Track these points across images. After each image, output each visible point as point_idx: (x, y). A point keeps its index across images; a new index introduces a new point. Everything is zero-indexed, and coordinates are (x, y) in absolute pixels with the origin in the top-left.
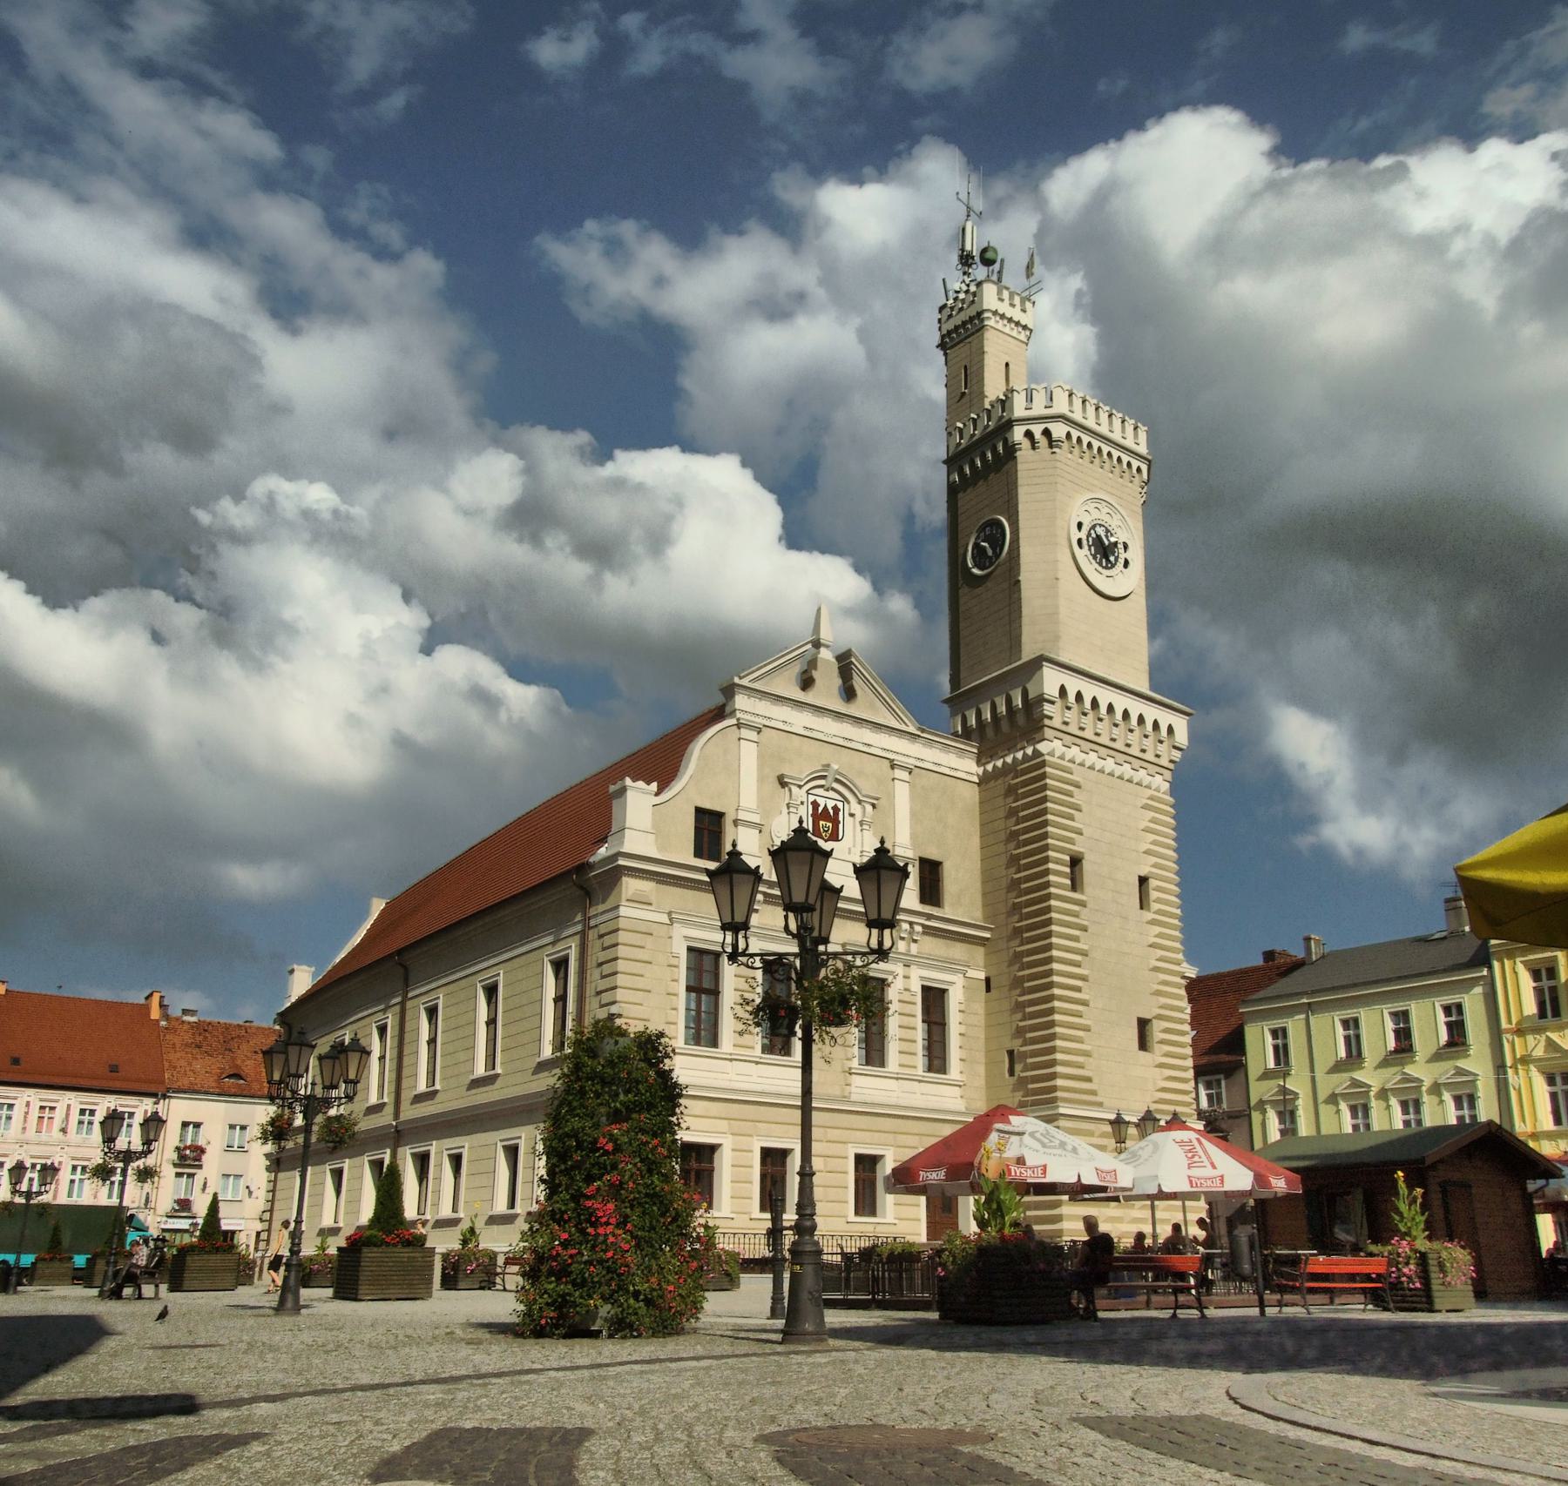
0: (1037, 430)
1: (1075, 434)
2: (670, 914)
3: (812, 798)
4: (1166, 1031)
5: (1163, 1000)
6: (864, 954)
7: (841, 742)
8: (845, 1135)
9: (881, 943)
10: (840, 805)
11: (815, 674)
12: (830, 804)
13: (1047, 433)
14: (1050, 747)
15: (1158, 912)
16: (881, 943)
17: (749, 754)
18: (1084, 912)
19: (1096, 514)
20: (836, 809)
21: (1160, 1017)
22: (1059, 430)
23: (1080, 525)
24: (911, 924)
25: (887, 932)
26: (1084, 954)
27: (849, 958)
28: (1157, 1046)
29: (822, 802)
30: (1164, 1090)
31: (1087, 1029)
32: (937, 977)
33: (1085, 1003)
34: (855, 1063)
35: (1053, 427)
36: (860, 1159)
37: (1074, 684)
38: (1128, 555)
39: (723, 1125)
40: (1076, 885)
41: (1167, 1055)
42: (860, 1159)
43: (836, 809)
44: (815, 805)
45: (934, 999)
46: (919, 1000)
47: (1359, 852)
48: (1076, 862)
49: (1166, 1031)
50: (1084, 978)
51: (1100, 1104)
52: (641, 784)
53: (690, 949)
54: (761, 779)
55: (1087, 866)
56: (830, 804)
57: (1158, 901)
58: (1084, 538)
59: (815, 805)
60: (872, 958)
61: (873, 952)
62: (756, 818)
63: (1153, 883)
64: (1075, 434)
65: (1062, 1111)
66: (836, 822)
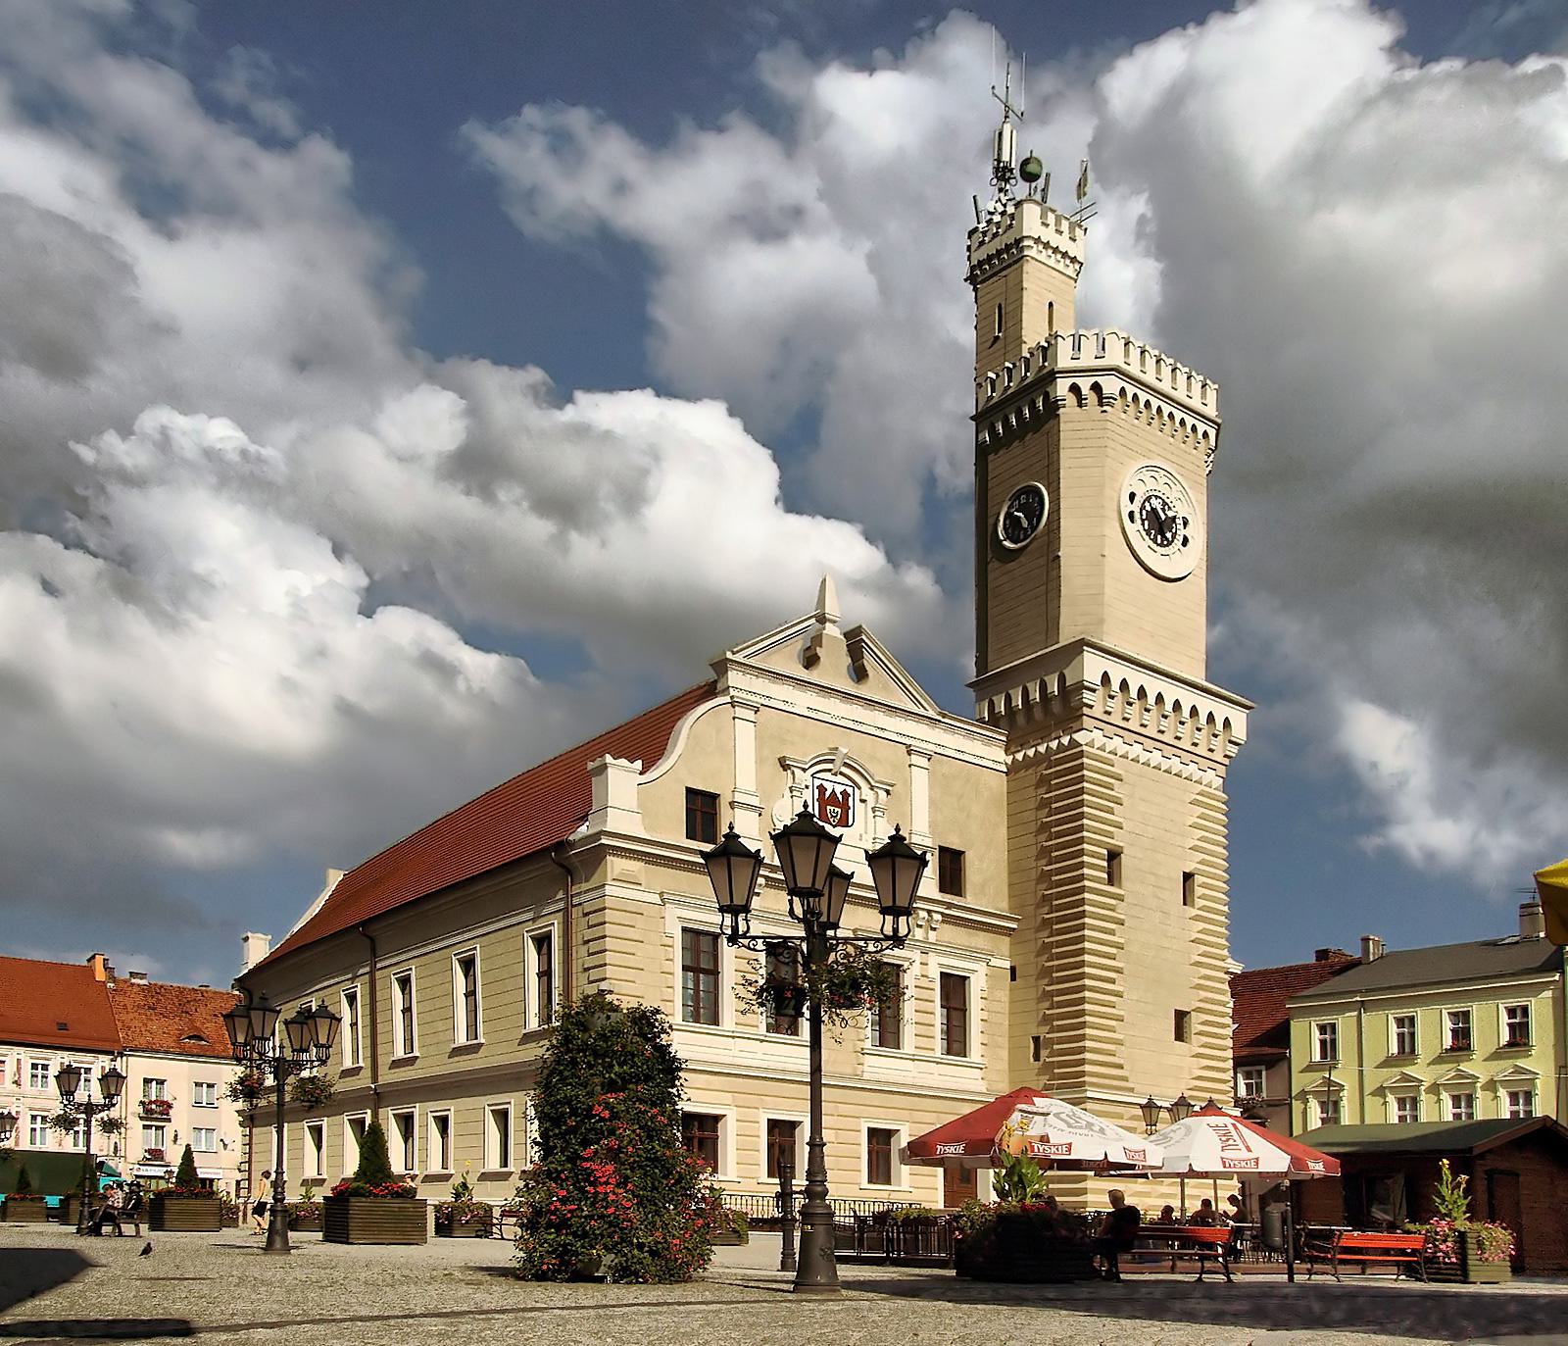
2: (661, 894)
3: (817, 782)
5: (1204, 994)
6: (877, 940)
7: (851, 725)
9: (896, 930)
10: (850, 790)
12: (839, 789)
13: (1096, 388)
16: (896, 930)
17: (745, 734)
19: (1151, 484)
20: (845, 794)
21: (1198, 1010)
22: (1111, 385)
23: (1132, 496)
25: (902, 920)
26: (1120, 947)
27: (862, 943)
29: (829, 786)
32: (957, 965)
37: (1118, 672)
38: (1187, 532)
43: (845, 794)
44: (822, 789)
48: (1114, 856)
50: (1119, 971)
51: (1132, 1090)
52: (623, 762)
53: (685, 930)
54: (760, 761)
56: (839, 789)
60: (885, 944)
61: (887, 938)
63: (1198, 879)
64: (1131, 390)
66: (845, 807)
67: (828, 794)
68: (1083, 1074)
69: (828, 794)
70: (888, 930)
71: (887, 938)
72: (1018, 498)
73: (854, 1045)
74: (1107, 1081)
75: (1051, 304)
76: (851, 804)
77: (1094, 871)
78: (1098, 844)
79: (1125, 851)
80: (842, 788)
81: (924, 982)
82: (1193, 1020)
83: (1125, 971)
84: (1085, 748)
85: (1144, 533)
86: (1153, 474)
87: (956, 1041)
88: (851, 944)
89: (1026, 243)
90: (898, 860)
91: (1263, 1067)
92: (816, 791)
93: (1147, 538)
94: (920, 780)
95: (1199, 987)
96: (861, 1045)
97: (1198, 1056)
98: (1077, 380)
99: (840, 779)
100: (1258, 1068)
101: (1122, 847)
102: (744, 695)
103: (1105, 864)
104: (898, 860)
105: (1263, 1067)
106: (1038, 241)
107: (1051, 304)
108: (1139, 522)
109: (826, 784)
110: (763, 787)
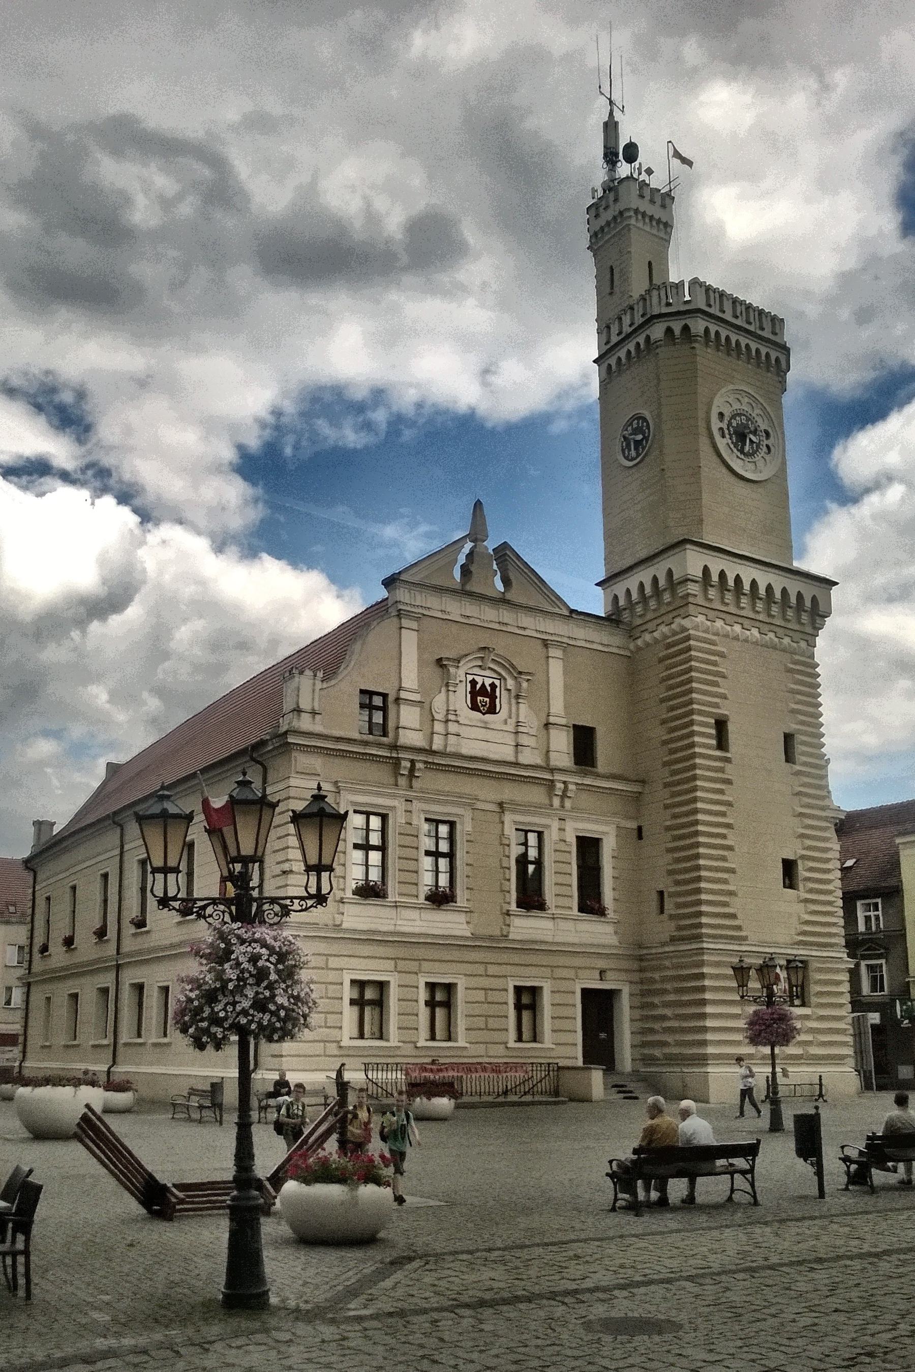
0: (677, 327)
1: (713, 328)
2: (336, 783)
3: (470, 678)
4: (811, 869)
5: (809, 842)
6: (302, 898)
7: (497, 626)
8: (509, 970)
9: (319, 888)
10: (497, 682)
11: (473, 568)
12: (488, 682)
13: (686, 328)
14: (697, 622)
15: (805, 764)
16: (319, 888)
17: (410, 640)
18: (728, 767)
19: (736, 406)
20: (493, 686)
21: (803, 857)
22: (698, 326)
23: (721, 415)
24: (564, 783)
25: (325, 875)
26: (729, 804)
27: (288, 902)
28: (801, 886)
29: (479, 680)
30: (804, 933)
31: (732, 871)
32: (590, 829)
33: (730, 848)
34: (513, 906)
35: (691, 323)
36: (518, 990)
37: (716, 564)
38: (769, 442)
39: (390, 965)
40: (722, 742)
41: (811, 891)
42: (518, 990)
43: (493, 686)
44: (474, 683)
45: (588, 848)
46: (574, 849)
47: (720, 229)
48: (721, 725)
49: (811, 869)
50: (728, 826)
51: (745, 938)
54: (421, 663)
55: (731, 727)
56: (488, 682)
57: (804, 754)
58: (725, 427)
59: (474, 683)
60: (310, 902)
61: (311, 897)
62: (416, 697)
63: (799, 738)
64: (713, 328)
65: (705, 945)
66: (493, 697)
67: (478, 686)
68: (700, 925)
69: (478, 686)
70: (313, 891)
71: (311, 897)
72: (631, 424)
73: (501, 907)
74: (719, 932)
75: (650, 263)
76: (498, 694)
77: (704, 738)
78: (709, 714)
79: (731, 719)
80: (491, 681)
81: (562, 846)
82: (800, 868)
83: (736, 827)
84: (691, 632)
85: (732, 446)
86: (738, 396)
87: (590, 902)
88: (279, 904)
89: (627, 214)
90: (325, 819)
91: (879, 901)
92: (469, 685)
93: (735, 450)
94: (556, 670)
95: (802, 836)
96: (506, 907)
97: (806, 901)
98: (671, 324)
99: (488, 673)
100: (874, 901)
101: (726, 715)
102: (409, 608)
103: (713, 732)
104: (325, 819)
105: (879, 901)
106: (636, 211)
107: (650, 263)
108: (728, 436)
109: (478, 679)
110: (423, 688)
